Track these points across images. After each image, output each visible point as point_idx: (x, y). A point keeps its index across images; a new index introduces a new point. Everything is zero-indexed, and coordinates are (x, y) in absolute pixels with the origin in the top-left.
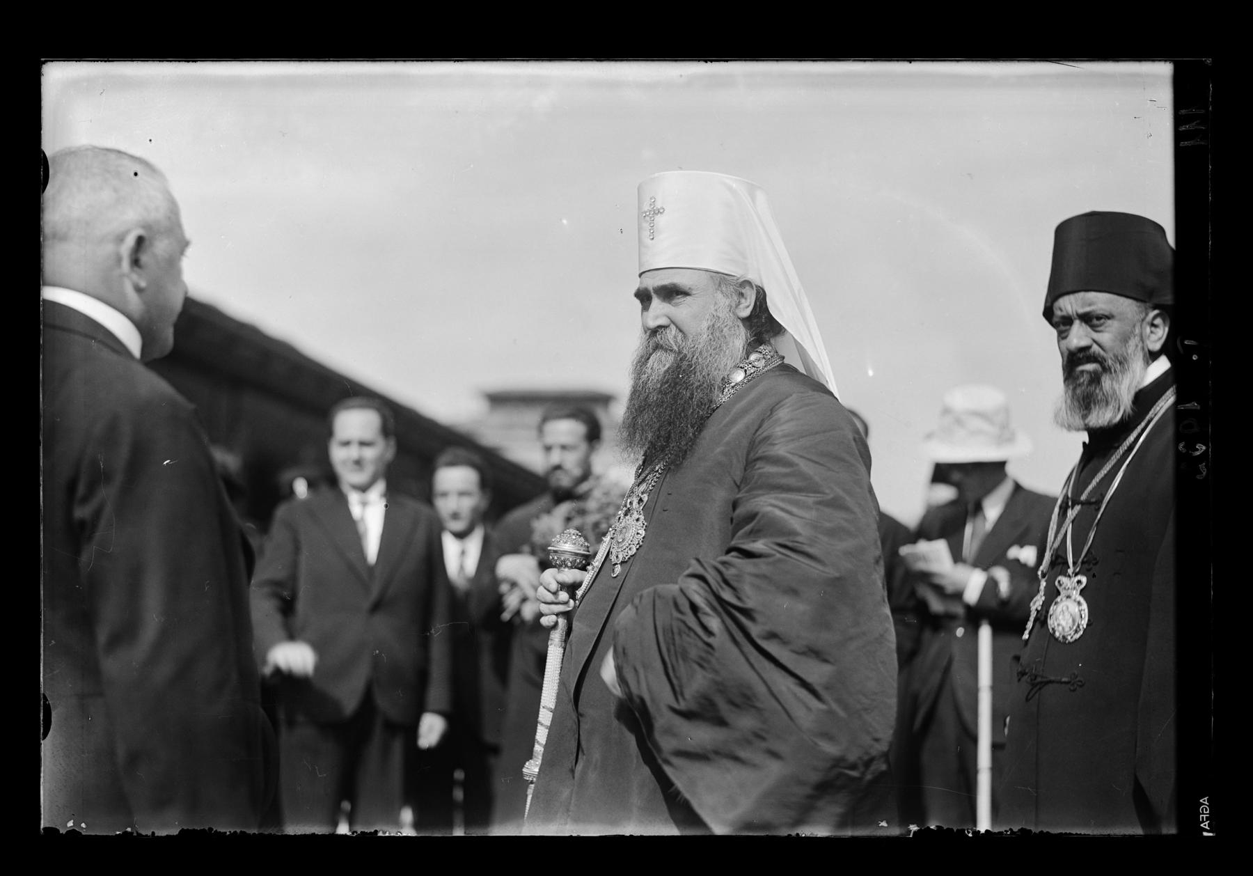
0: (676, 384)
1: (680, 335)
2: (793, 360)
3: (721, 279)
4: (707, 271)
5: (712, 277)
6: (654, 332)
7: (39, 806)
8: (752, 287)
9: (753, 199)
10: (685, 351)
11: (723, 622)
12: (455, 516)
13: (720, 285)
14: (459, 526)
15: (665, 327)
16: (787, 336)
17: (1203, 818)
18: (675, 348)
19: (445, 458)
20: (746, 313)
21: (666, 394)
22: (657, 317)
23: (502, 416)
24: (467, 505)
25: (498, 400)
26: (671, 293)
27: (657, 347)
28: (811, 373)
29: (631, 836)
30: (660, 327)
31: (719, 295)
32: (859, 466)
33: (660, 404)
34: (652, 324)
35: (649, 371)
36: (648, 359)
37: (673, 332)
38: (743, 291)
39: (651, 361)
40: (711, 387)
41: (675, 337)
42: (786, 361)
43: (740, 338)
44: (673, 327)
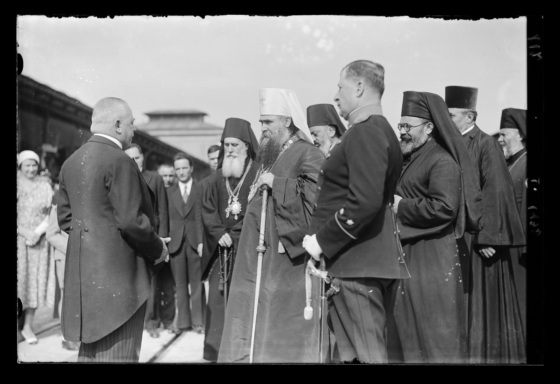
0: (270, 146)
1: (271, 133)
2: (302, 137)
3: (281, 117)
4: (277, 115)
5: (278, 117)
6: (264, 132)
7: (16, 280)
8: (290, 118)
9: (288, 95)
10: (272, 137)
11: (483, 157)
12: (182, 175)
13: (280, 119)
14: (184, 179)
15: (267, 131)
16: (300, 131)
17: (22, 23)
18: (269, 137)
19: (177, 157)
20: (288, 126)
21: (267, 149)
22: (264, 128)
23: (155, 124)
24: (186, 172)
25: (153, 116)
26: (268, 122)
27: (265, 136)
28: (307, 139)
29: (476, 18)
30: (265, 131)
31: (280, 122)
32: (325, 280)
33: (265, 151)
34: (264, 130)
35: (263, 142)
36: (263, 139)
37: (269, 132)
38: (287, 120)
39: (264, 139)
40: (279, 146)
41: (269, 134)
42: (301, 138)
43: (287, 134)
44: (269, 131)
